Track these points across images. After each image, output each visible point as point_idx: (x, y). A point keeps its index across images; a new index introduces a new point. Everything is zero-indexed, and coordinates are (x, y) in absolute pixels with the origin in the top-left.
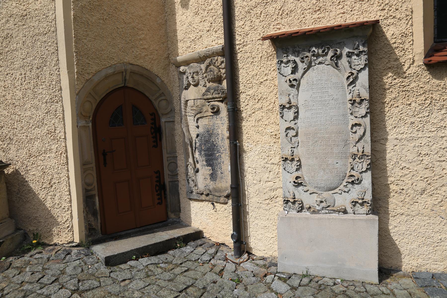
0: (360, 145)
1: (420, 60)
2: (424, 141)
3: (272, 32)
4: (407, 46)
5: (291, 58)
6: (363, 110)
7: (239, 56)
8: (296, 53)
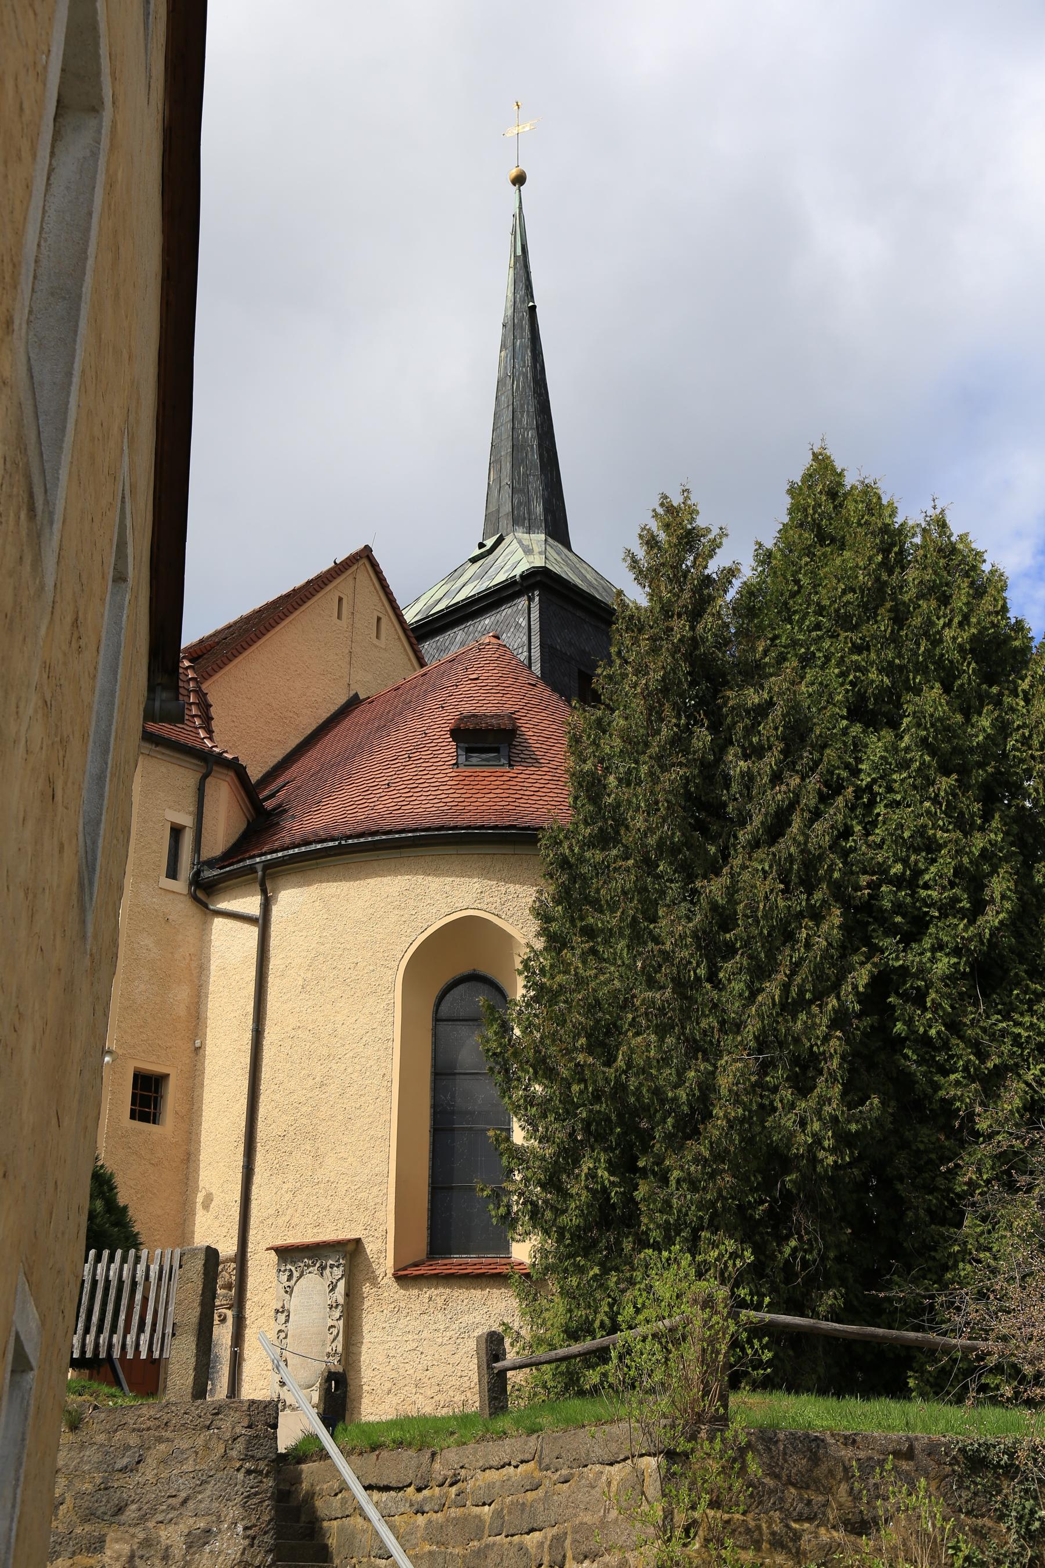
0: (334, 1345)
1: (390, 1271)
2: (392, 1344)
3: (279, 1242)
4: (382, 1260)
5: (289, 1267)
6: (337, 1314)
7: (249, 1263)
8: (293, 1263)
